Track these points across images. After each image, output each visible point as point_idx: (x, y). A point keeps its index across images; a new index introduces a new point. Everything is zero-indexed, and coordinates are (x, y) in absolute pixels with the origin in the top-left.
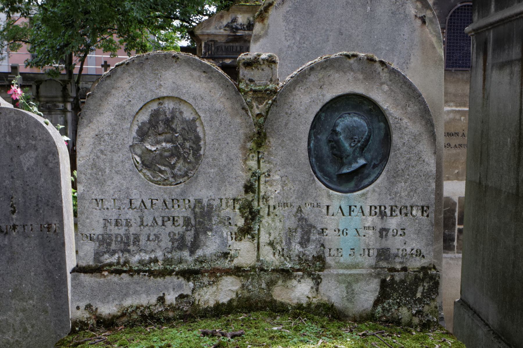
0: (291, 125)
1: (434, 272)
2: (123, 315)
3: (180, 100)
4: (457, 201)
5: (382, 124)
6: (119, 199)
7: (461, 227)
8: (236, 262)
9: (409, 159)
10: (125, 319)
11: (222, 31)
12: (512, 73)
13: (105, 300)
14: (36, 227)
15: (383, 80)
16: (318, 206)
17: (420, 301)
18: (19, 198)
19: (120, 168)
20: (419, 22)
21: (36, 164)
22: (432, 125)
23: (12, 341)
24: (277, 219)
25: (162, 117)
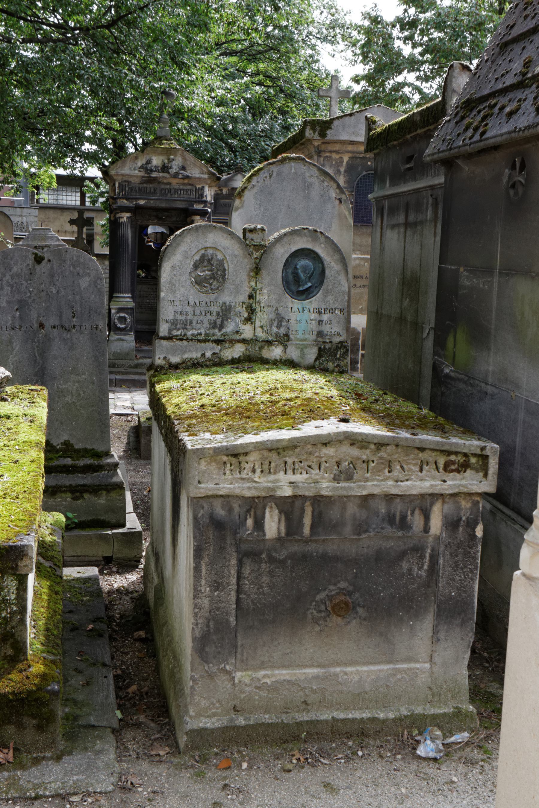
0: (273, 264)
1: (346, 344)
2: (183, 363)
3: (216, 249)
4: (361, 331)
5: (320, 265)
6: (183, 301)
7: (363, 352)
8: (243, 336)
9: (334, 284)
10: (184, 365)
11: (137, 172)
12: (399, 233)
13: (174, 354)
14: (89, 327)
15: (322, 241)
16: (287, 307)
17: (339, 359)
18: (77, 308)
19: (184, 284)
20: (337, 202)
21: (89, 286)
22: (347, 266)
23: (70, 402)
24: (265, 314)
25: (206, 258)
